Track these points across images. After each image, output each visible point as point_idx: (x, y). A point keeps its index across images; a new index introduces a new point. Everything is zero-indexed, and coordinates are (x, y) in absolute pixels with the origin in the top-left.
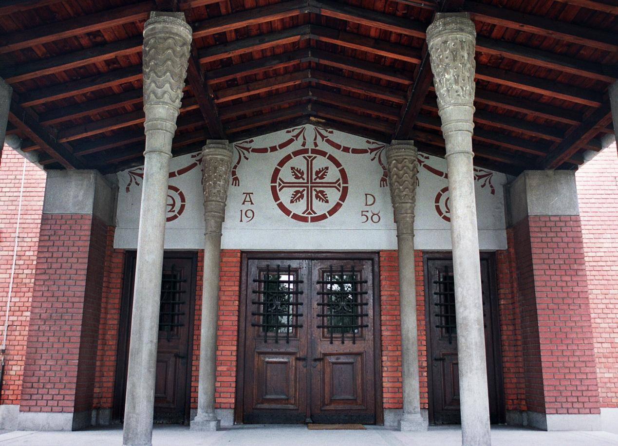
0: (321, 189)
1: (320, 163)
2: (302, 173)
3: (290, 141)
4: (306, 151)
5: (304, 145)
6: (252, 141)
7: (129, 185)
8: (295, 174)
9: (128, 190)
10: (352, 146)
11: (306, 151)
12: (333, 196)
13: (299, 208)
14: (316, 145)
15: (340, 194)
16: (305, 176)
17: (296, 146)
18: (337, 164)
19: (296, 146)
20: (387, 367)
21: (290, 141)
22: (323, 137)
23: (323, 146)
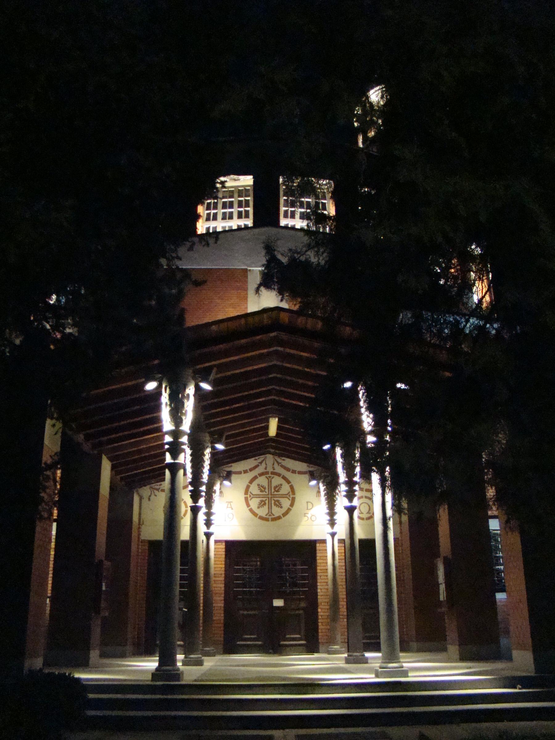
0: (262, 493)
1: (277, 481)
2: (265, 488)
3: (256, 467)
4: (267, 473)
5: (266, 469)
6: (231, 466)
7: (150, 496)
8: (260, 489)
9: (149, 499)
10: (298, 469)
11: (267, 473)
12: (263, 512)
13: (286, 503)
14: (274, 469)
15: (264, 515)
16: (267, 490)
17: (261, 469)
18: (288, 482)
19: (261, 469)
20: (321, 616)
21: (256, 467)
22: (278, 463)
23: (278, 469)
